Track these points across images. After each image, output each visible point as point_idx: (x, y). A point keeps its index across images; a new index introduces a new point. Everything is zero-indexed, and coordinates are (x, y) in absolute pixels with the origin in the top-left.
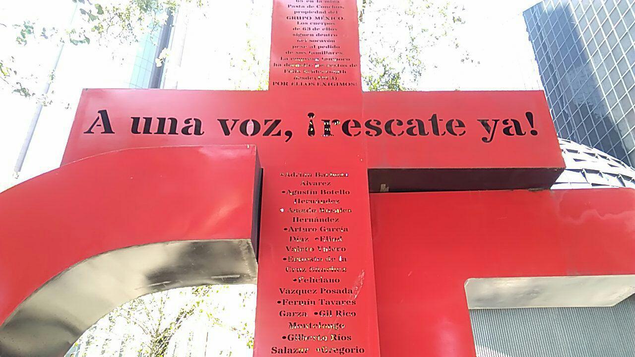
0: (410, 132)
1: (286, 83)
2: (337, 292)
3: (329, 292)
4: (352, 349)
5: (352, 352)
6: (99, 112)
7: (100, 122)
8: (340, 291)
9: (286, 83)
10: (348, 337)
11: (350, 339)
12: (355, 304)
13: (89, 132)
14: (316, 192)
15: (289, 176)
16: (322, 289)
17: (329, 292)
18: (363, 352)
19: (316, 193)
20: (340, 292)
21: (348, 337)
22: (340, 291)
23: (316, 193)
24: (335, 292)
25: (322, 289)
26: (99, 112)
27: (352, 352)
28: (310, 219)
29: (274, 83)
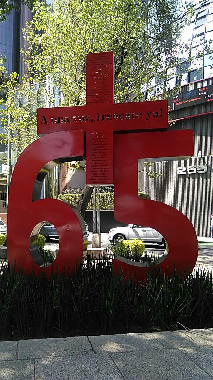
7: (44, 120)
13: (42, 123)
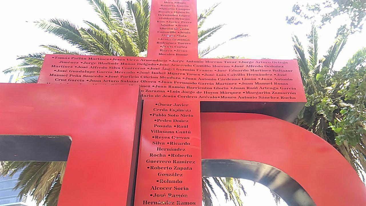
0: (167, 105)
1: (248, 88)
2: (163, 127)
3: (159, 126)
4: (182, 188)
5: (182, 190)
6: (286, 20)
8: (165, 126)
9: (248, 88)
10: (194, 203)
11: (195, 204)
12: (189, 139)
14: (100, 81)
15: (174, 40)
16: (155, 125)
17: (159, 126)
18: (191, 157)
19: (100, 81)
20: (165, 127)
21: (194, 203)
22: (165, 126)
23: (100, 81)
24: (164, 132)
25: (155, 125)
26: (286, 20)
27: (182, 190)
28: (168, 149)
29: (72, 58)
